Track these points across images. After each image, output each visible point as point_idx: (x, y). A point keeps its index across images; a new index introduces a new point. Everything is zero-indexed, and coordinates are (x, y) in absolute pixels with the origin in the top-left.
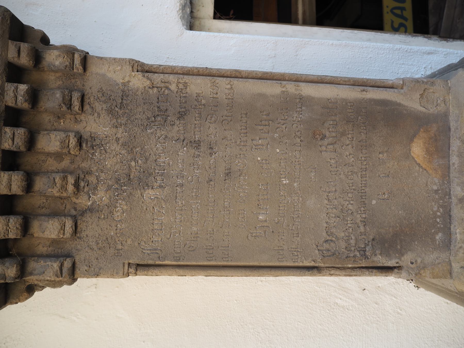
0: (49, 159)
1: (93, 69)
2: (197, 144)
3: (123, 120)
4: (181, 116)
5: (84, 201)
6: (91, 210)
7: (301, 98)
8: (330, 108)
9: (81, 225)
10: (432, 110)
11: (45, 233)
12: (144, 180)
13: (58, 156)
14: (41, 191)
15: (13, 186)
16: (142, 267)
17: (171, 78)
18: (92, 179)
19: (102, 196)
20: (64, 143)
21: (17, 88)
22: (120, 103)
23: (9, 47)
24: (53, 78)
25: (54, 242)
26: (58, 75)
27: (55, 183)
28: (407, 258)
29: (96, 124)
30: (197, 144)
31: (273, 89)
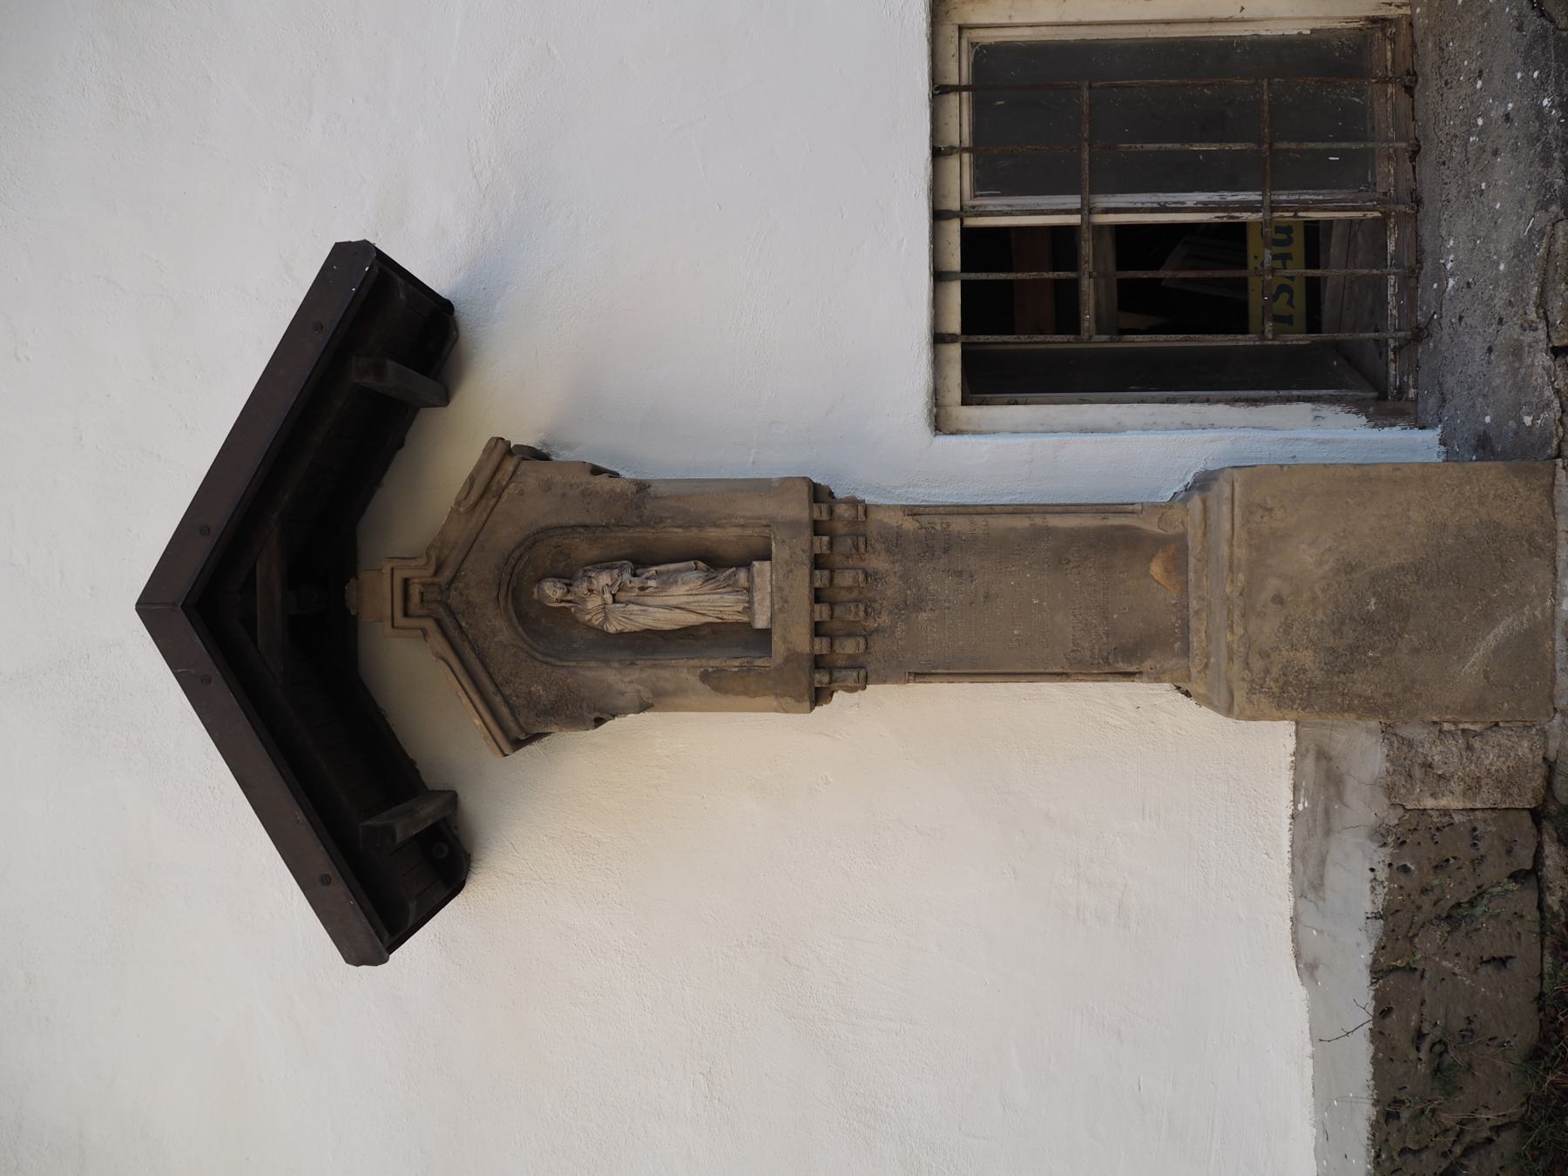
1: (873, 516)
2: (960, 574)
3: (898, 557)
4: (946, 551)
5: (872, 624)
6: (877, 630)
7: (1048, 528)
8: (1074, 537)
9: (871, 643)
10: (1171, 532)
12: (918, 606)
13: (850, 589)
16: (920, 675)
17: (936, 519)
18: (877, 606)
19: (885, 619)
20: (855, 579)
22: (895, 542)
25: (850, 656)
28: (1147, 665)
29: (878, 562)
30: (960, 574)
31: (1021, 523)
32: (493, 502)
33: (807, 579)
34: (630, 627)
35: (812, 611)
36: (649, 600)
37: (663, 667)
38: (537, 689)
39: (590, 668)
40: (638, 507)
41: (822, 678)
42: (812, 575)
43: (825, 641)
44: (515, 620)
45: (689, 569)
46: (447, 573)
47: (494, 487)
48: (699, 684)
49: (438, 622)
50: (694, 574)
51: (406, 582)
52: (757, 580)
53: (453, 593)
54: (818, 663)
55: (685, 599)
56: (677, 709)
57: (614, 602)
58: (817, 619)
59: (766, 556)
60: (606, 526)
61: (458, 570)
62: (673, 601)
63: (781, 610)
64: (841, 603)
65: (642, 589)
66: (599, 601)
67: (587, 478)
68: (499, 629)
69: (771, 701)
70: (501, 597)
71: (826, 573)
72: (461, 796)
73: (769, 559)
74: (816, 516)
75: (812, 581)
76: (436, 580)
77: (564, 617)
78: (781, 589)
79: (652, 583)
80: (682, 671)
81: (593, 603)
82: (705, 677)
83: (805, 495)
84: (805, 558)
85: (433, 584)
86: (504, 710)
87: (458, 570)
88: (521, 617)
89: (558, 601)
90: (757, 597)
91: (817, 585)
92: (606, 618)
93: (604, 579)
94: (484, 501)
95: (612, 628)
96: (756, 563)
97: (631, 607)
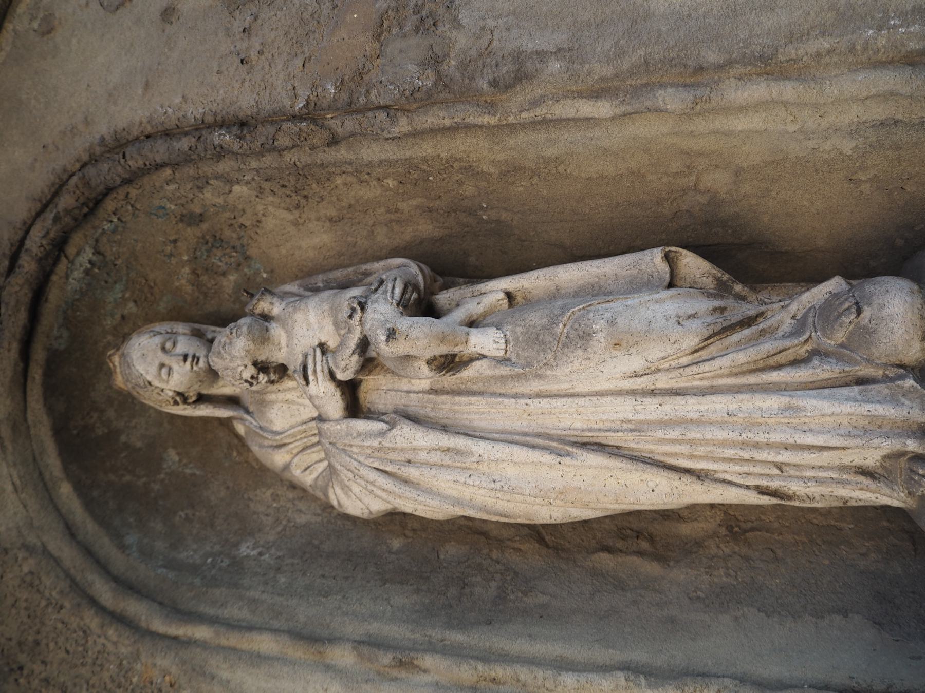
36: (475, 411)
39: (257, 659)
44: (53, 462)
45: (640, 285)
50: (665, 306)
55: (624, 409)
60: (311, 114)
62: (572, 418)
65: (449, 363)
77: (215, 442)
79: (485, 341)
83: (708, 508)
89: (182, 397)
95: (361, 499)
97: (408, 436)
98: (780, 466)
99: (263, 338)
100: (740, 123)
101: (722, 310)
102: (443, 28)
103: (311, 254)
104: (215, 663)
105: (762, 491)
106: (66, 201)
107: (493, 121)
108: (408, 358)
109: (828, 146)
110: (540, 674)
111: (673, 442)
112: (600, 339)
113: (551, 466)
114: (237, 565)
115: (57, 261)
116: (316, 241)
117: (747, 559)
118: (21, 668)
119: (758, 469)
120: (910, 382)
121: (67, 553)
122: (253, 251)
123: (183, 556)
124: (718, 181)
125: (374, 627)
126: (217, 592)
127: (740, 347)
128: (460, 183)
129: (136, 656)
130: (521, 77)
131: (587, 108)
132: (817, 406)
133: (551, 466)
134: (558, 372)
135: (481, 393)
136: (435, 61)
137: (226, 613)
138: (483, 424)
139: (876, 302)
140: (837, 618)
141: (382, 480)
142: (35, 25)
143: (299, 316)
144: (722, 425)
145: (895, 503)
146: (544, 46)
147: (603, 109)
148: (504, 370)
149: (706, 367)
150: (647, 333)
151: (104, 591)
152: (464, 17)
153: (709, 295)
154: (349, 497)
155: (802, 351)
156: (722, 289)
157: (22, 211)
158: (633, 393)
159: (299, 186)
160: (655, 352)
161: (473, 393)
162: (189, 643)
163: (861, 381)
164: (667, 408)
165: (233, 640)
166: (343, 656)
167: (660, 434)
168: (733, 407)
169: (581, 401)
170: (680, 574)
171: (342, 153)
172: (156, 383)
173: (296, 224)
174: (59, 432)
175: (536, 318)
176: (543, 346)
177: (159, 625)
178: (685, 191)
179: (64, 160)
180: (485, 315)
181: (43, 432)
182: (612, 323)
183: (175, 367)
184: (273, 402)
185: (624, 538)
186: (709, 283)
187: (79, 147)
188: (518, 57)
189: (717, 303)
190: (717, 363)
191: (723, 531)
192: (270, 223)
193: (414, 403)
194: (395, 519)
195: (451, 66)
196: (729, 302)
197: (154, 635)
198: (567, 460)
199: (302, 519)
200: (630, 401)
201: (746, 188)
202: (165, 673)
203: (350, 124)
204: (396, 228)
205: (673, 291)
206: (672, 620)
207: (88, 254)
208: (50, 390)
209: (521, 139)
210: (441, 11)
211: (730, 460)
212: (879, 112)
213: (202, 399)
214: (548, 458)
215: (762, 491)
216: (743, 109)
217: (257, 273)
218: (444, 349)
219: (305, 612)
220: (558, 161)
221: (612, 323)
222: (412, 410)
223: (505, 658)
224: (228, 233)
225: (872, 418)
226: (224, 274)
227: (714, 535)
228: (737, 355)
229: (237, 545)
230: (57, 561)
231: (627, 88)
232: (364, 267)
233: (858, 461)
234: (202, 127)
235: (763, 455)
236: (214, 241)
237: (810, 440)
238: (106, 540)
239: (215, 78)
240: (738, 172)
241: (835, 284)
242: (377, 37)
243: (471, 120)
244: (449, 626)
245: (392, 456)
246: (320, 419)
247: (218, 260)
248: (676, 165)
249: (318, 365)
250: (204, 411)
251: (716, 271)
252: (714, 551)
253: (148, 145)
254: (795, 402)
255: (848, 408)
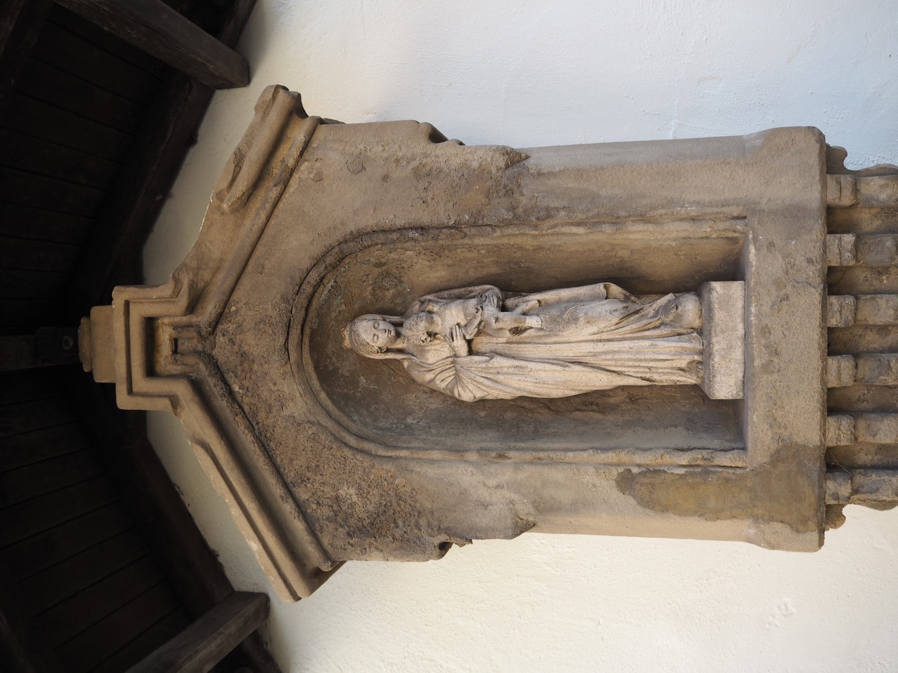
0: (869, 332)
11: (878, 437)
13: (884, 329)
14: (866, 379)
15: (843, 376)
21: (840, 240)
23: (829, 184)
24: (867, 216)
25: (883, 448)
26: (874, 211)
27: (890, 368)
32: (274, 193)
33: (817, 312)
34: (495, 393)
35: (825, 370)
36: (527, 350)
37: (552, 463)
38: (348, 492)
39: (432, 462)
40: (509, 193)
41: (837, 486)
42: (824, 305)
43: (845, 422)
44: (315, 383)
45: (594, 298)
46: (210, 309)
47: (276, 169)
48: (615, 494)
49: (197, 387)
50: (605, 307)
51: (150, 325)
52: (719, 315)
53: (221, 340)
54: (835, 463)
56: (575, 530)
57: (471, 352)
58: (833, 383)
59: (732, 270)
60: (456, 227)
61: (226, 303)
62: (567, 352)
63: (766, 368)
64: (870, 353)
65: (517, 331)
66: (446, 352)
67: (424, 146)
68: (287, 396)
69: (746, 526)
70: (292, 347)
71: (849, 300)
72: (271, 595)
73: (742, 278)
74: (832, 197)
75: (824, 318)
76: (194, 319)
77: (391, 372)
78: (765, 331)
79: (533, 321)
80: (583, 470)
81: (436, 353)
82: (626, 481)
83: (814, 160)
84: (813, 274)
85: (189, 326)
86: (298, 526)
87: (226, 303)
88: (327, 376)
90: (718, 344)
91: (833, 322)
92: (457, 379)
93: (452, 315)
94: (261, 194)
95: (468, 393)
96: (717, 286)
97: (498, 361)
98: (649, 368)
99: (431, 322)
100: (633, 236)
101: (627, 307)
102: (517, 195)
103: (434, 280)
104: (412, 465)
105: (643, 379)
106: (330, 260)
107: (536, 233)
108: (501, 329)
109: (666, 243)
110: (559, 453)
111: (609, 360)
112: (582, 320)
113: (560, 371)
114: (408, 427)
115: (319, 286)
116: (439, 274)
117: (638, 410)
118: (309, 479)
119: (641, 370)
120: (695, 334)
121: (330, 424)
122: (404, 279)
123: (381, 424)
124: (625, 254)
125: (484, 445)
126: (405, 438)
127: (634, 322)
128: (515, 252)
129: (373, 466)
130: (549, 216)
131: (575, 230)
132: (662, 344)
133: (560, 371)
134: (564, 333)
135: (530, 343)
136: (513, 209)
137: (412, 445)
138: (531, 356)
139: (683, 304)
140: (673, 428)
141: (486, 382)
142: (312, 176)
143: (448, 312)
144: (628, 352)
145: (694, 382)
146: (558, 206)
147: (581, 230)
148: (541, 333)
149: (621, 330)
150: (599, 317)
151: (352, 441)
152: (525, 191)
153: (622, 301)
154: (464, 390)
155: (658, 323)
156: (626, 299)
157: (306, 264)
158: (592, 341)
159: (437, 254)
160: (602, 325)
161: (526, 343)
162: (398, 458)
163: (679, 334)
164: (606, 346)
165: (421, 455)
166: (473, 456)
167: (603, 357)
168: (632, 345)
169: (572, 345)
170: (610, 417)
171: (466, 241)
172: (371, 343)
173: (430, 267)
174: (316, 368)
175: (554, 312)
176: (558, 323)
177: (381, 452)
178: (611, 257)
179: (332, 240)
180: (529, 310)
181: (310, 368)
182: (586, 314)
183: (380, 335)
184: (429, 350)
185: (586, 405)
186: (622, 297)
187: (339, 235)
188: (548, 209)
189: (625, 305)
190: (625, 328)
191: (628, 400)
192: (417, 267)
193: (499, 348)
194: (482, 401)
195: (520, 210)
196: (629, 304)
197: (376, 456)
198: (567, 369)
199: (433, 407)
200: (592, 344)
201: (635, 257)
202: (388, 471)
203: (473, 230)
204: (480, 269)
205: (608, 301)
206: (609, 433)
207: (332, 283)
208: (312, 348)
209: (546, 238)
210: (515, 188)
211: (631, 366)
212: (684, 234)
213: (388, 350)
214: (559, 368)
215: (643, 379)
216: (635, 232)
217: (405, 289)
218: (516, 325)
219: (450, 442)
220: (559, 246)
221: (586, 314)
222: (498, 351)
223: (542, 450)
224: (394, 270)
225: (683, 348)
226: (388, 290)
227: (624, 402)
228: (633, 325)
229: (405, 419)
230: (326, 428)
231: (592, 223)
232: (470, 289)
233: (679, 366)
234: (401, 230)
235: (643, 364)
236: (388, 274)
237: (660, 357)
238: (345, 418)
239: (410, 208)
240: (632, 251)
241: (670, 296)
242: (487, 197)
243: (528, 232)
244: (516, 441)
245: (491, 371)
246: (455, 356)
247: (386, 283)
248: (608, 248)
249: (458, 333)
250: (390, 356)
251: (625, 292)
252: (624, 408)
253: (375, 236)
254: (654, 343)
255: (674, 344)
